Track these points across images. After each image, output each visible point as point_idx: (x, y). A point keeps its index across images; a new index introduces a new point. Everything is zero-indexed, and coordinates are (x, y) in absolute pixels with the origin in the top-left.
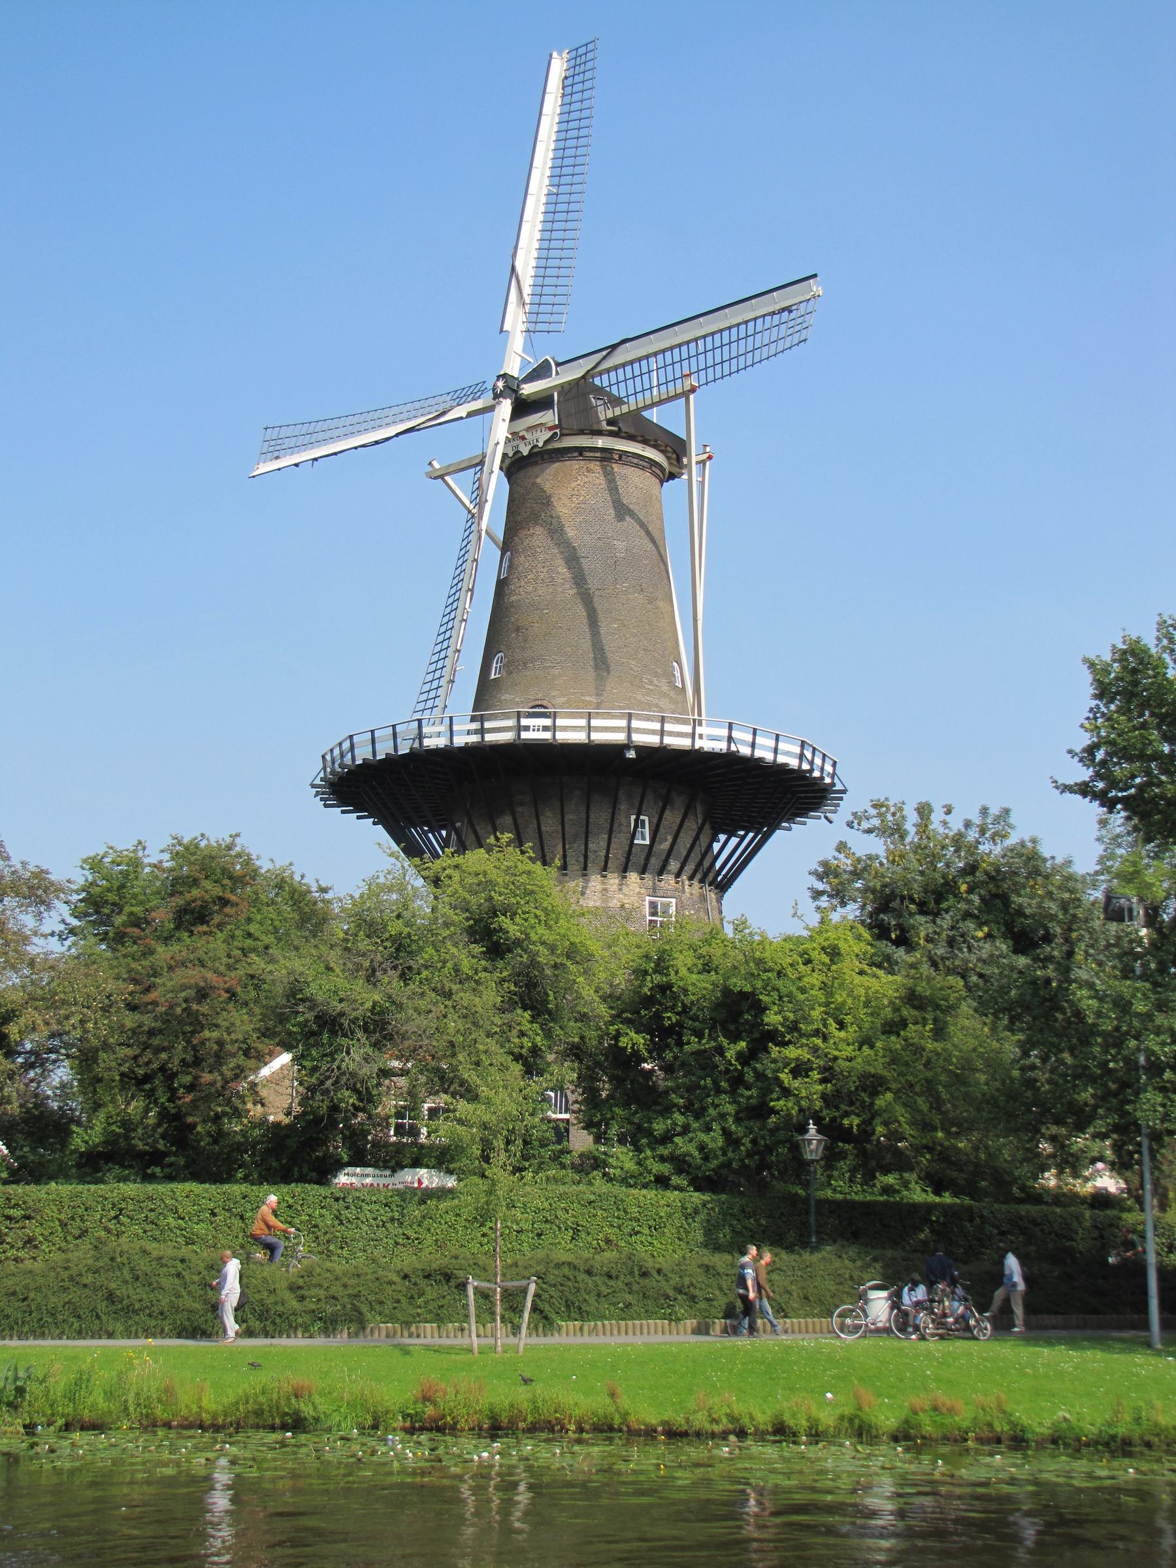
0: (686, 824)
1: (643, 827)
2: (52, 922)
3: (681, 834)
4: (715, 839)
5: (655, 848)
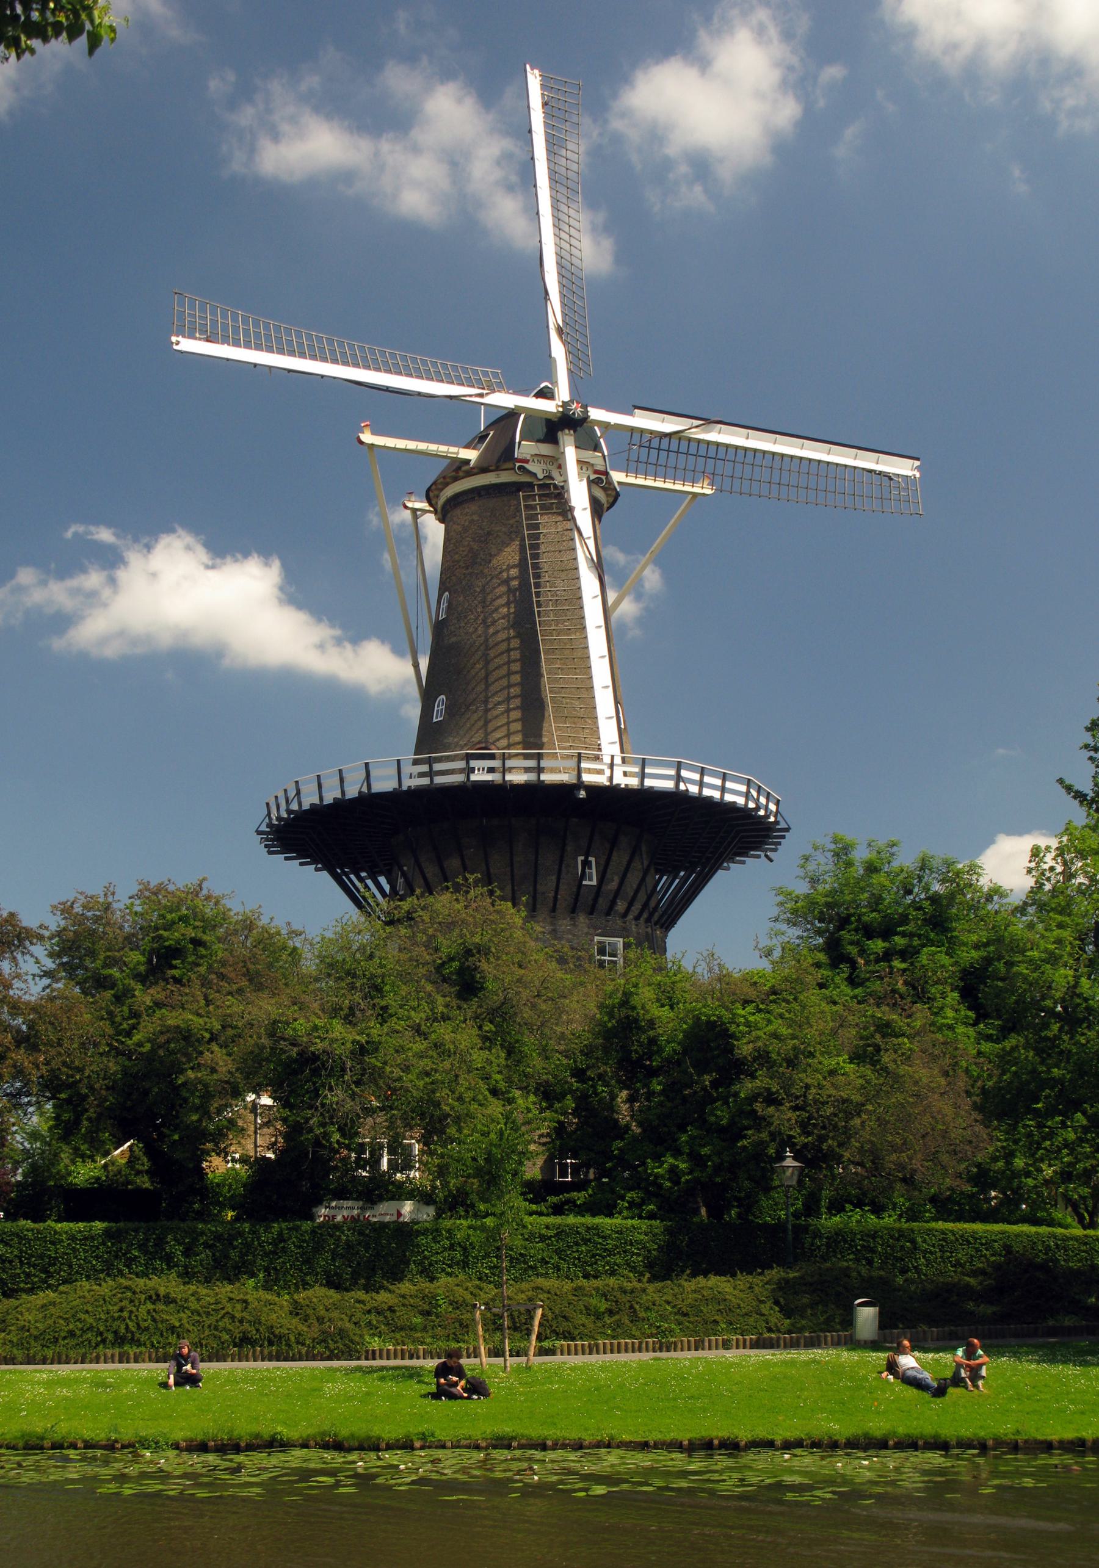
0: (633, 865)
1: (590, 868)
2: (28, 966)
3: (629, 875)
5: (604, 888)
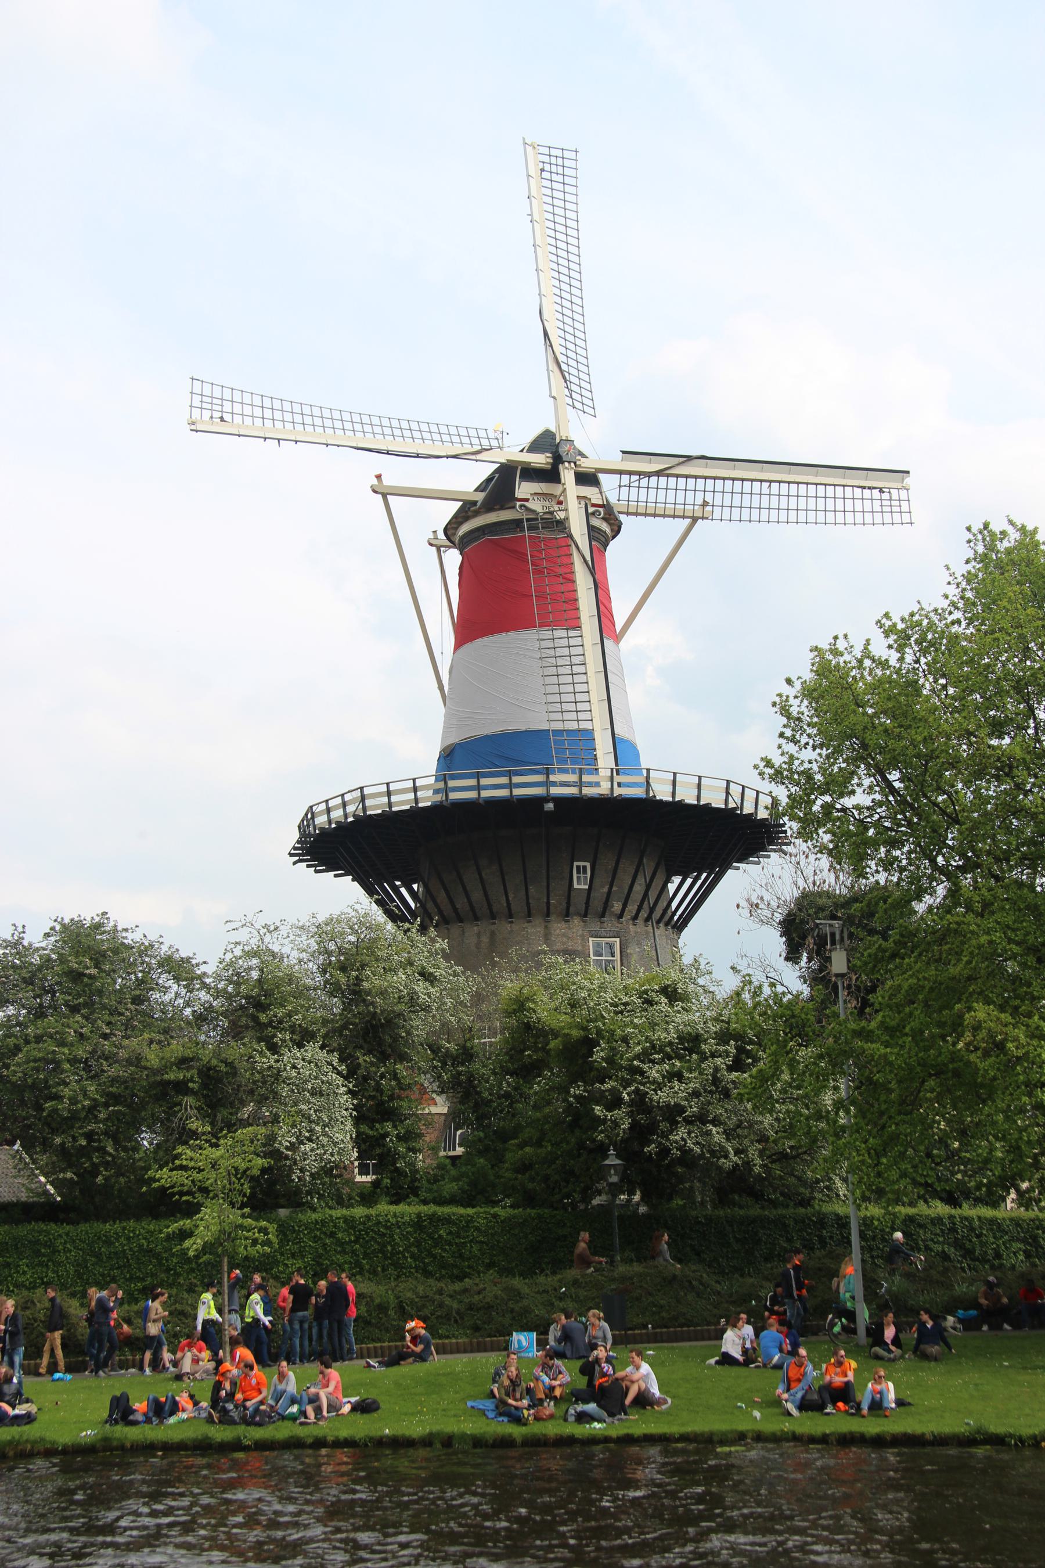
4: (668, 880)
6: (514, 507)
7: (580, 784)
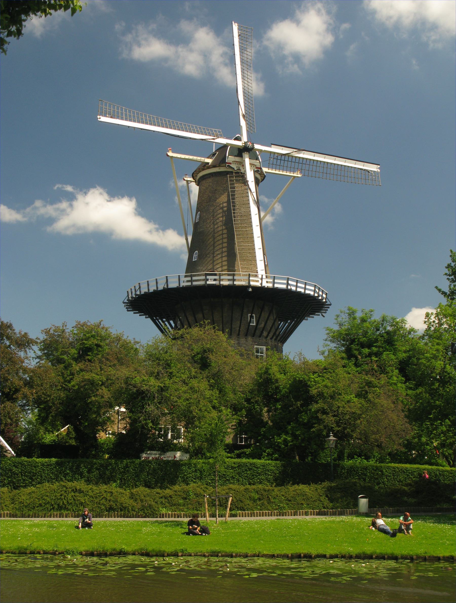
1: (253, 318)
2: (31, 354)
3: (268, 322)
6: (226, 166)
7: (234, 280)
